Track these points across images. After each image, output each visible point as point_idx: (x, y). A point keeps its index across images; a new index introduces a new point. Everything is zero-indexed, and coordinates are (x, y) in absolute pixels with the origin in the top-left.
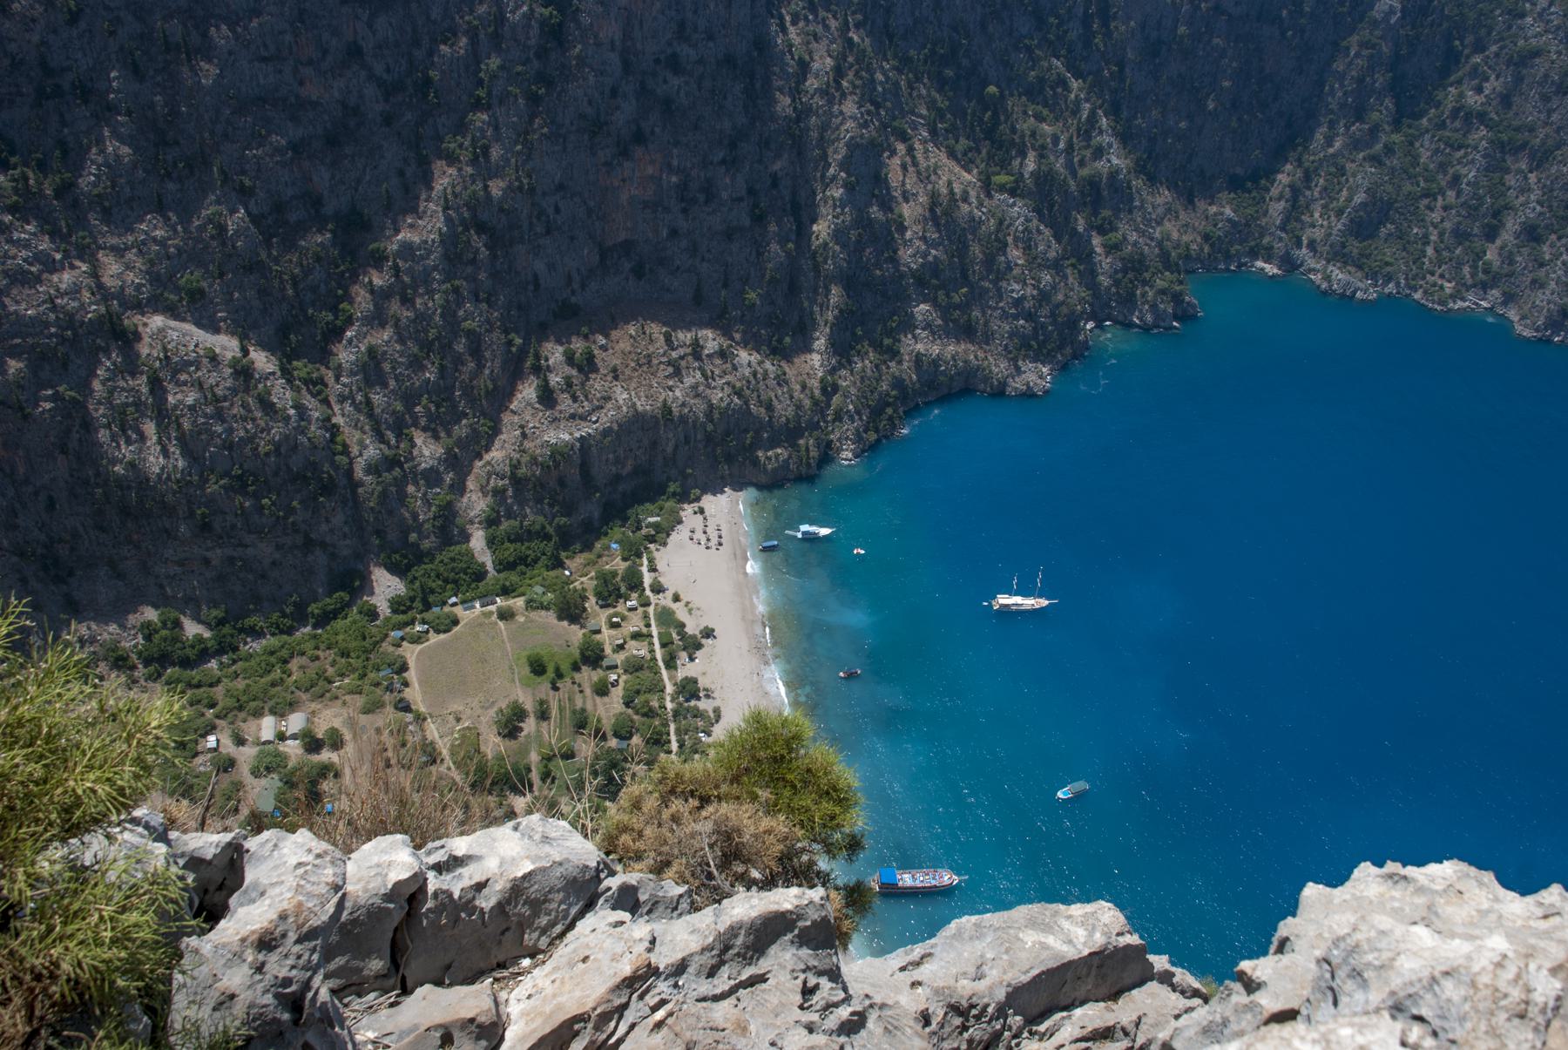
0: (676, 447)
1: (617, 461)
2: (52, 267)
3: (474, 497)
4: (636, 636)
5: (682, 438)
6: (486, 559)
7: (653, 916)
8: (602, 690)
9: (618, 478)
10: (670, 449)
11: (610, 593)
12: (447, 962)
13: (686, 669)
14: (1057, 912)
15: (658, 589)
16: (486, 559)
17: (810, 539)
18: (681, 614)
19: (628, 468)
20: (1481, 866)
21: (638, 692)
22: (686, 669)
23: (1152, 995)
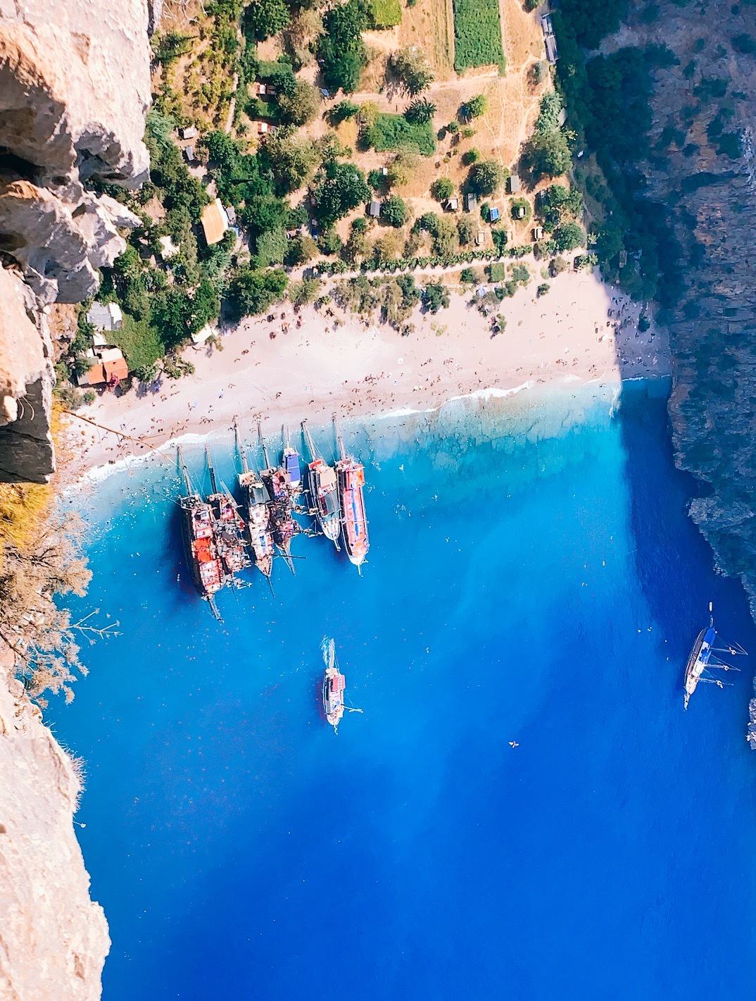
0: (722, 297)
1: (711, 222)
2: (197, 512)
3: (680, 33)
4: (500, 238)
5: (734, 305)
6: (606, 48)
8: (439, 192)
9: (691, 222)
10: (720, 289)
11: (546, 207)
12: (90, 46)
13: (458, 297)
14: (750, 285)
15: (553, 270)
16: (606, 48)
19: (701, 237)
20: (88, 867)
21: (435, 234)
22: (458, 297)
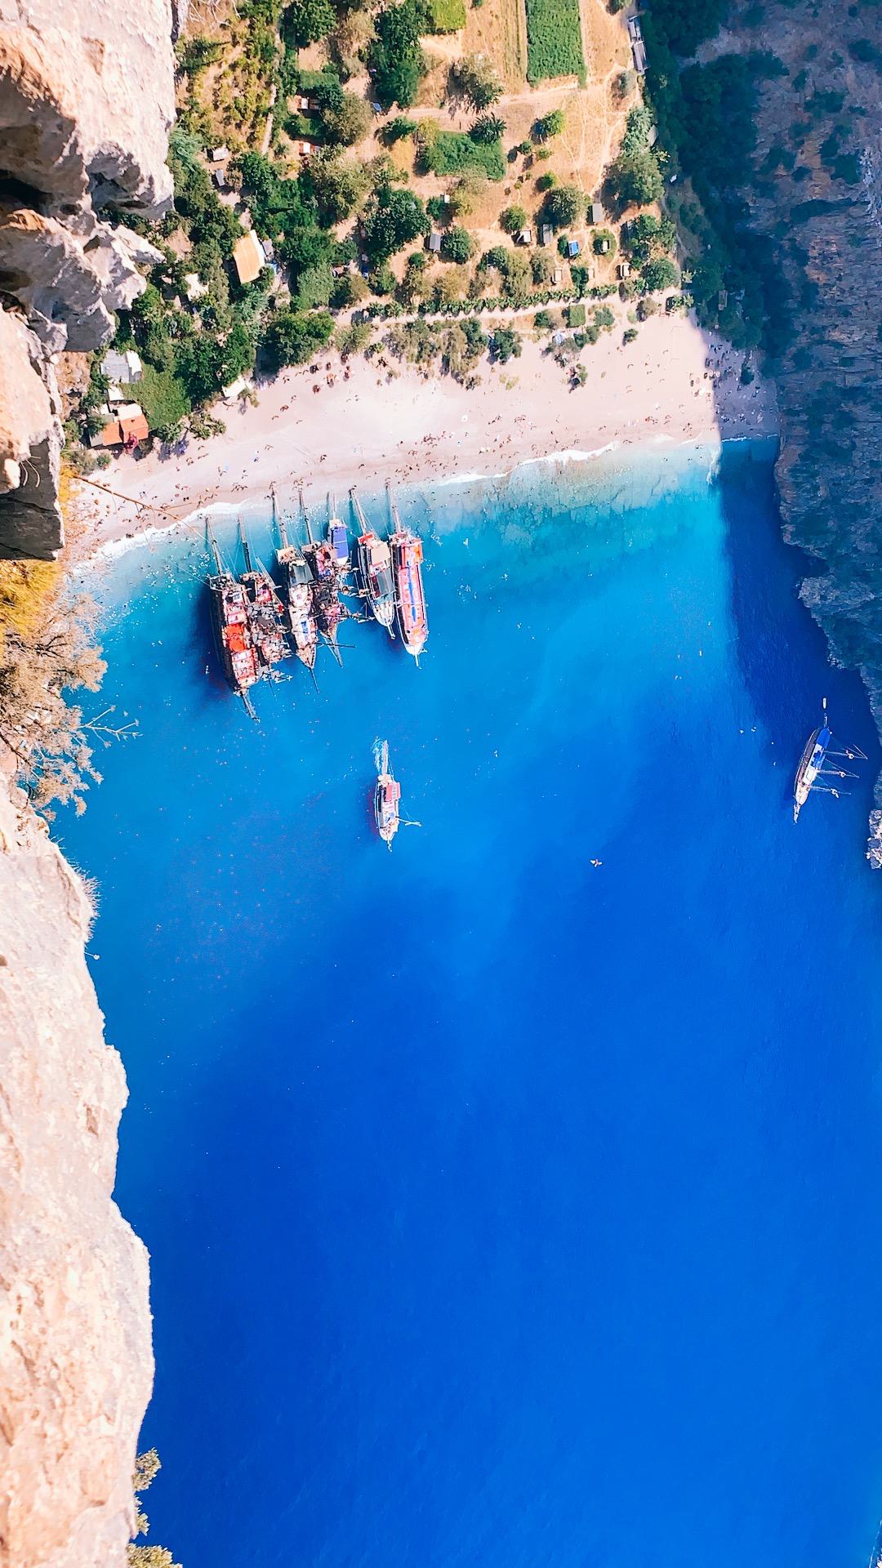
0: (838, 345)
1: (825, 257)
3: (790, 38)
4: (580, 276)
5: (851, 354)
6: (704, 55)
7: (183, 601)
8: (509, 222)
9: (802, 258)
10: (836, 335)
11: (634, 241)
13: (531, 345)
15: (641, 313)
16: (704, 55)
17: (372, 797)
18: (609, 340)
19: (814, 275)
21: (505, 271)
22: (531, 345)
23: (81, 103)
